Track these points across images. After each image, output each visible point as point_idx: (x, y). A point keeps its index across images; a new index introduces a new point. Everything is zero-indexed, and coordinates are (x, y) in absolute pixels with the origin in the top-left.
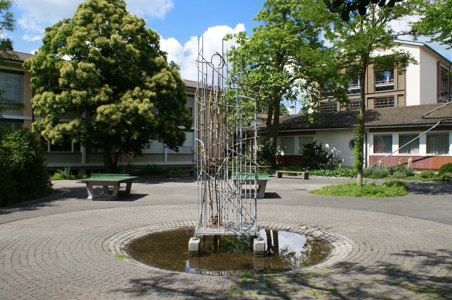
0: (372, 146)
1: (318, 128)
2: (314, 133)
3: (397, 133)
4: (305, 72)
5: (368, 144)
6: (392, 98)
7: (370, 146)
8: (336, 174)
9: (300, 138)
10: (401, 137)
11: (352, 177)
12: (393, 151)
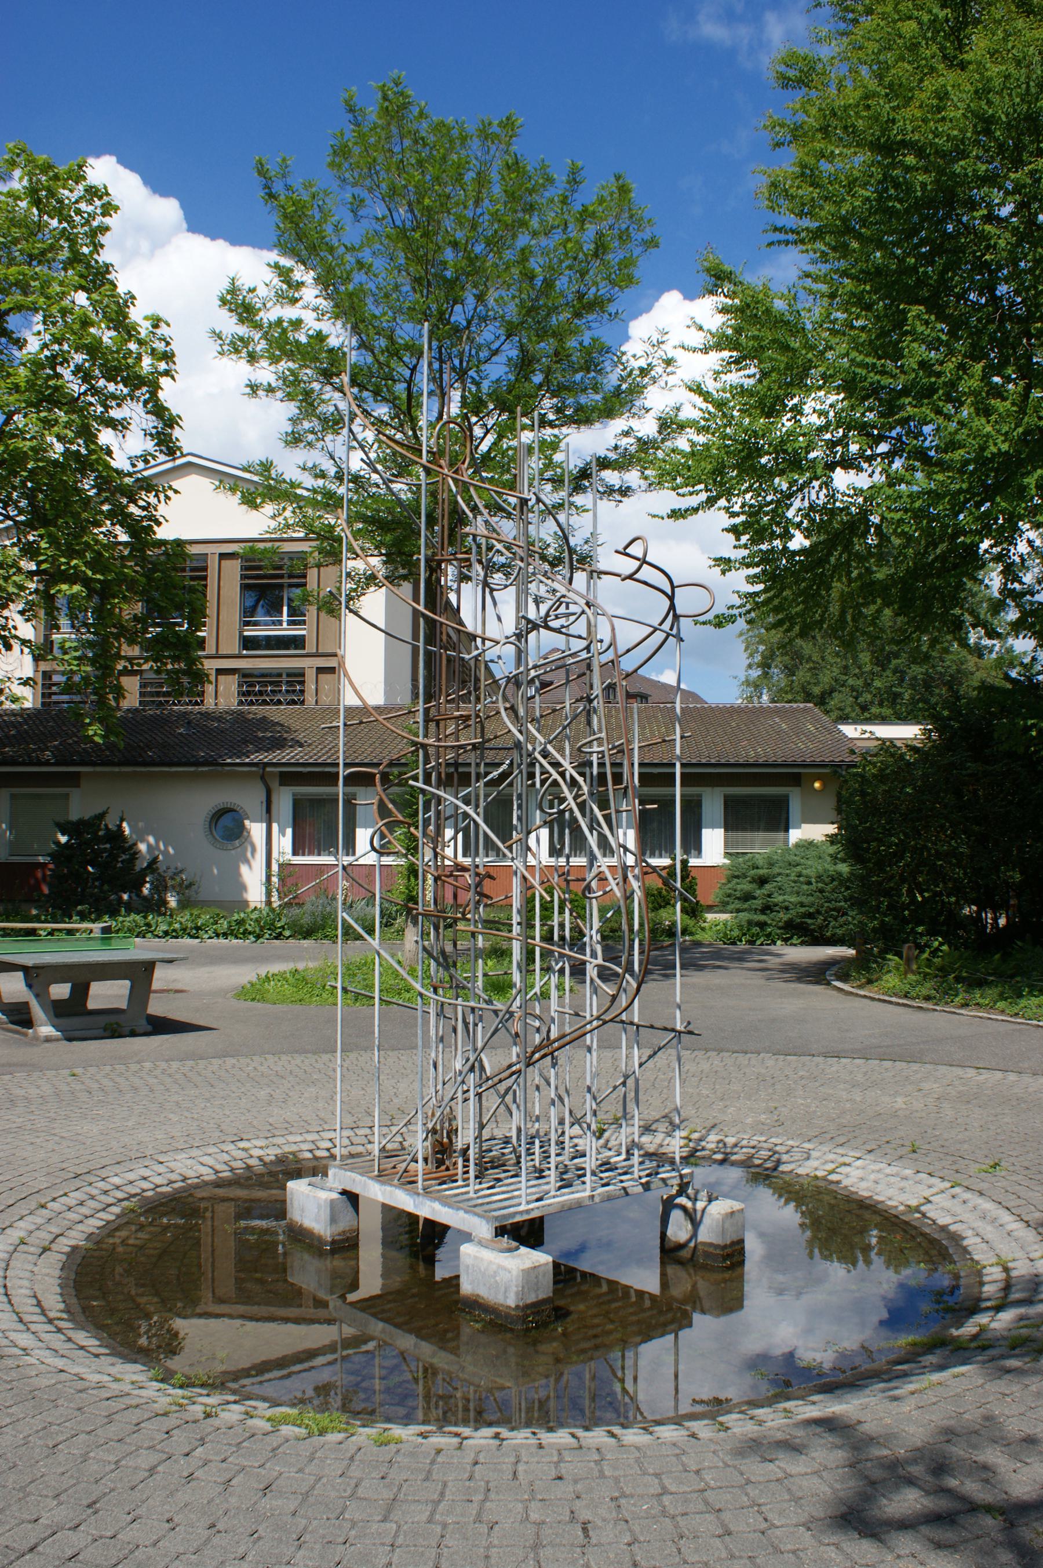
0: (289, 832)
1: (94, 764)
2: (74, 780)
3: (717, 790)
4: (88, 555)
5: (275, 827)
6: (297, 677)
7: (282, 832)
8: (198, 928)
9: (13, 797)
10: (297, 804)
11: (258, 937)
12: (358, 853)
